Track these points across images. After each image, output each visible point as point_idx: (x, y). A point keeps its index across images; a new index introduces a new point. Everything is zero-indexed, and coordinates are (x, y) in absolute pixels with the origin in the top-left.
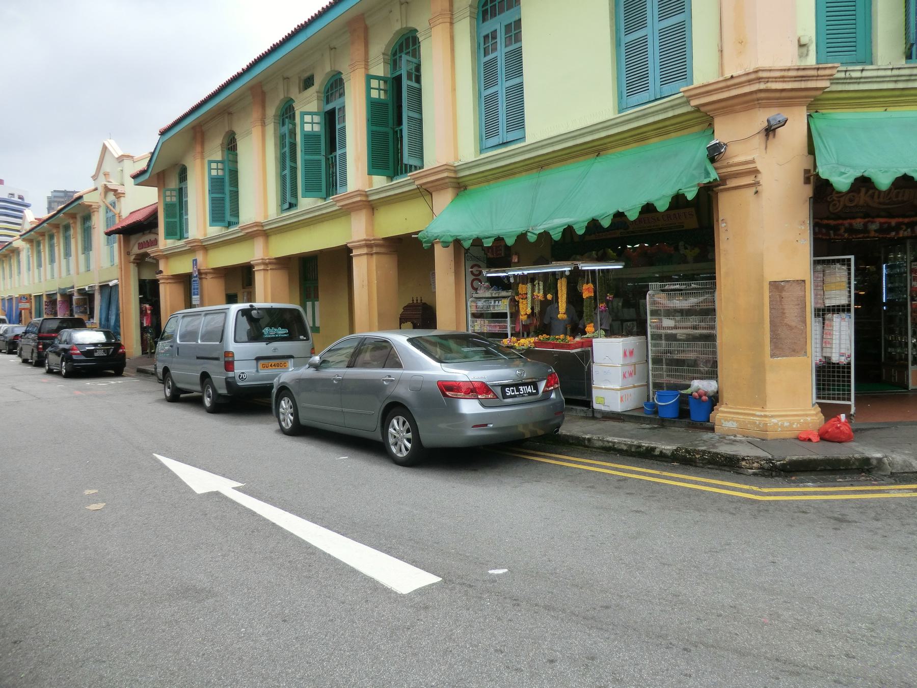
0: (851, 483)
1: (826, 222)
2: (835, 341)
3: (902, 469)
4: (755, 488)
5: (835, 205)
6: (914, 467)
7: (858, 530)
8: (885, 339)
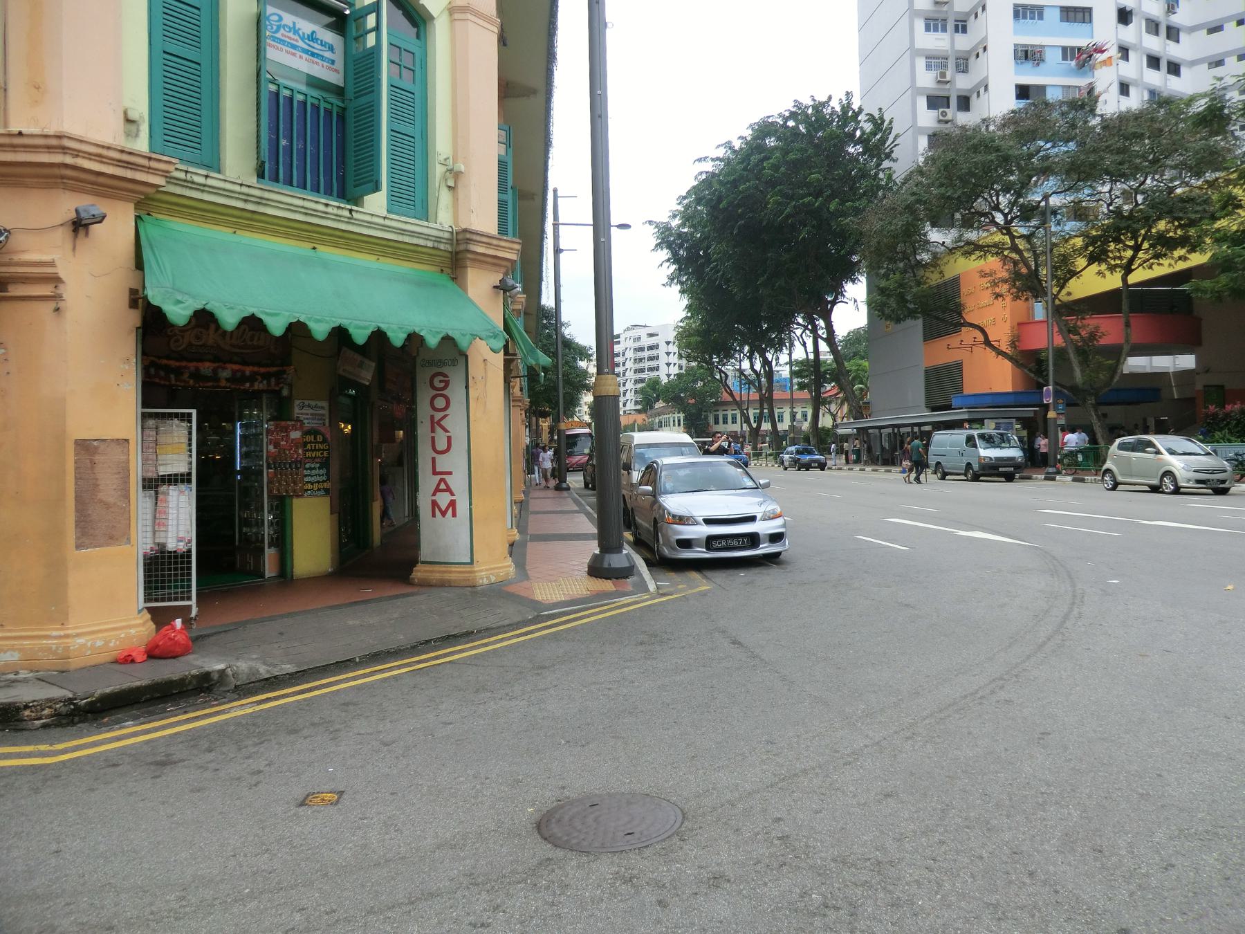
0: (185, 710)
1: (165, 362)
2: (172, 522)
3: (247, 679)
4: (43, 748)
5: (177, 341)
6: (261, 674)
7: (185, 770)
8: (239, 516)
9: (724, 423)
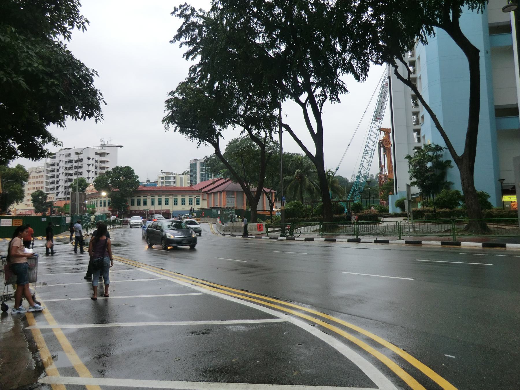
9: (138, 205)
